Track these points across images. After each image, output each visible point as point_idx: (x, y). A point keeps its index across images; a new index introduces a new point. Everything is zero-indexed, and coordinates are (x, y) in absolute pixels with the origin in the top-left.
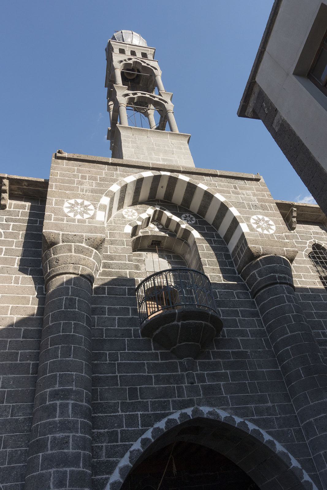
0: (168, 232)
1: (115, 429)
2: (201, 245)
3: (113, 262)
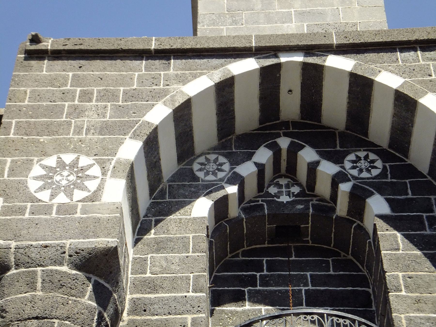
0: (315, 202)
2: (390, 235)
3: (156, 295)
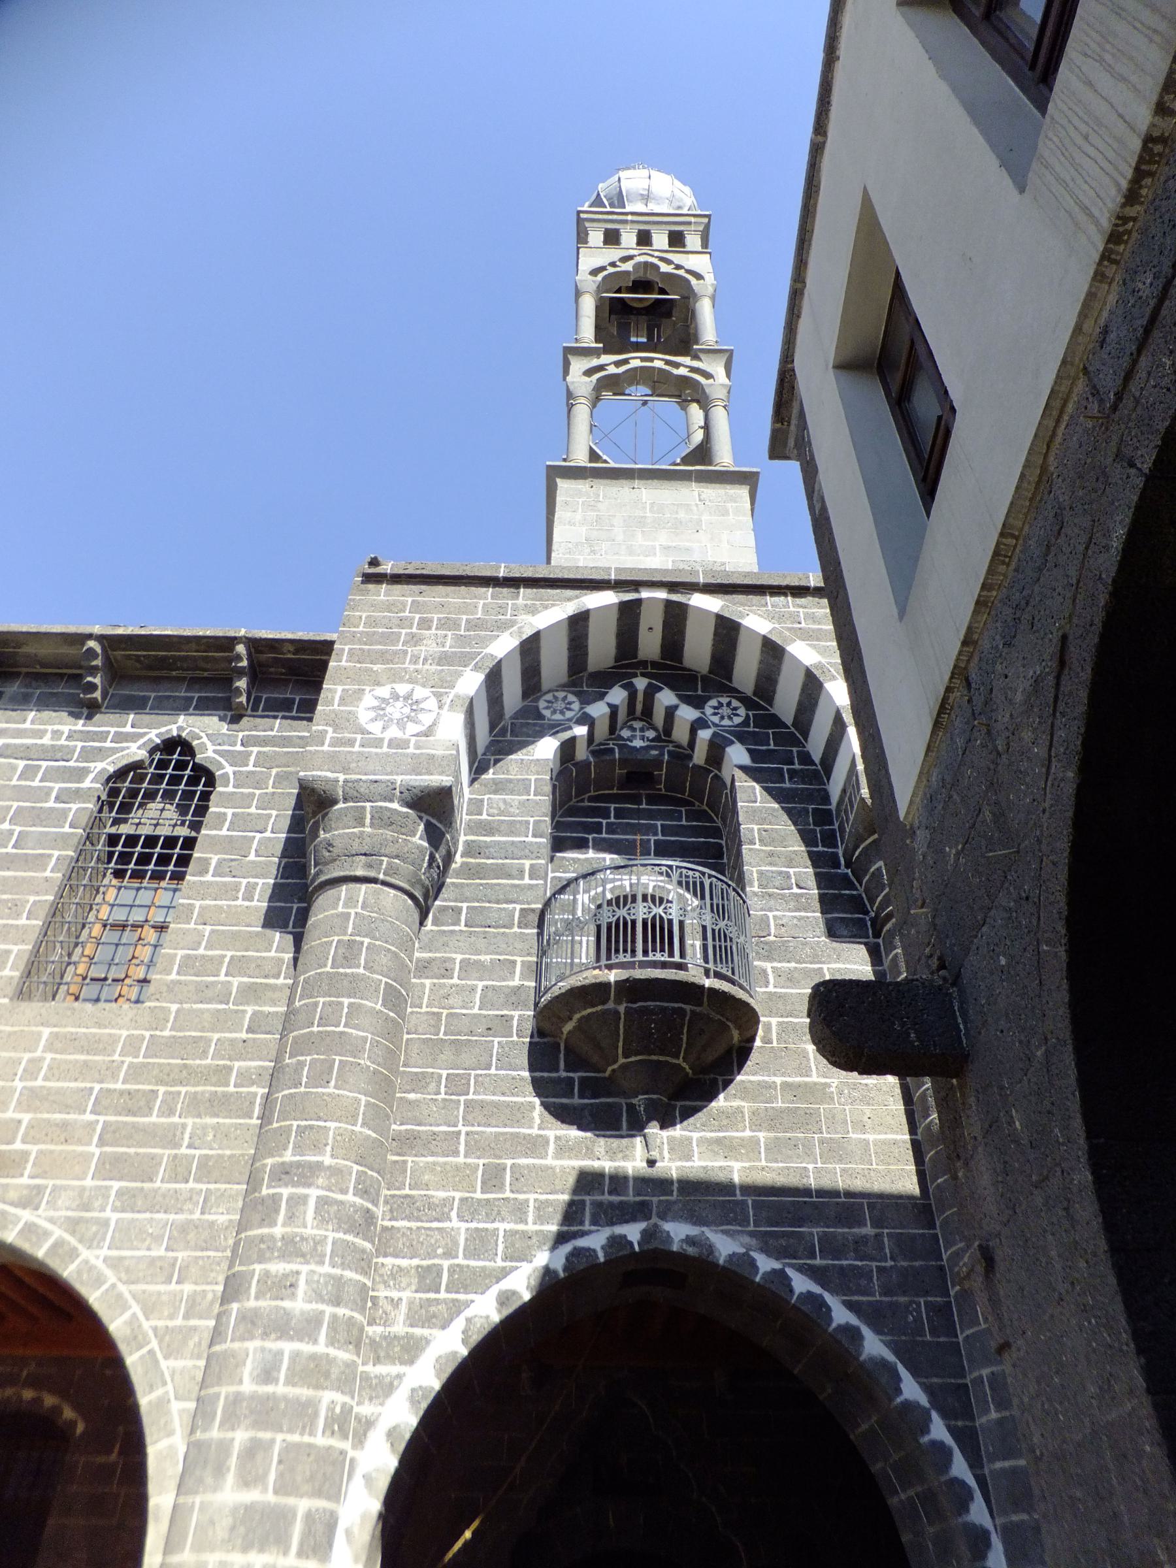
1: (436, 1261)
